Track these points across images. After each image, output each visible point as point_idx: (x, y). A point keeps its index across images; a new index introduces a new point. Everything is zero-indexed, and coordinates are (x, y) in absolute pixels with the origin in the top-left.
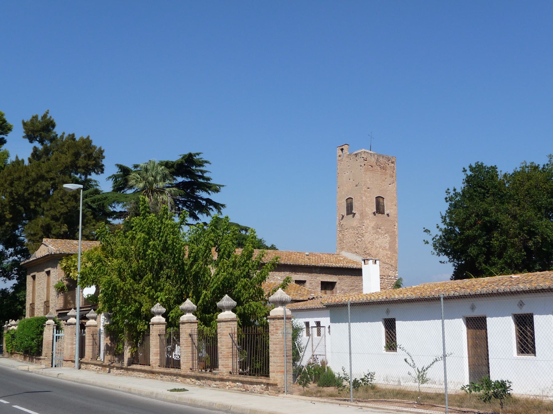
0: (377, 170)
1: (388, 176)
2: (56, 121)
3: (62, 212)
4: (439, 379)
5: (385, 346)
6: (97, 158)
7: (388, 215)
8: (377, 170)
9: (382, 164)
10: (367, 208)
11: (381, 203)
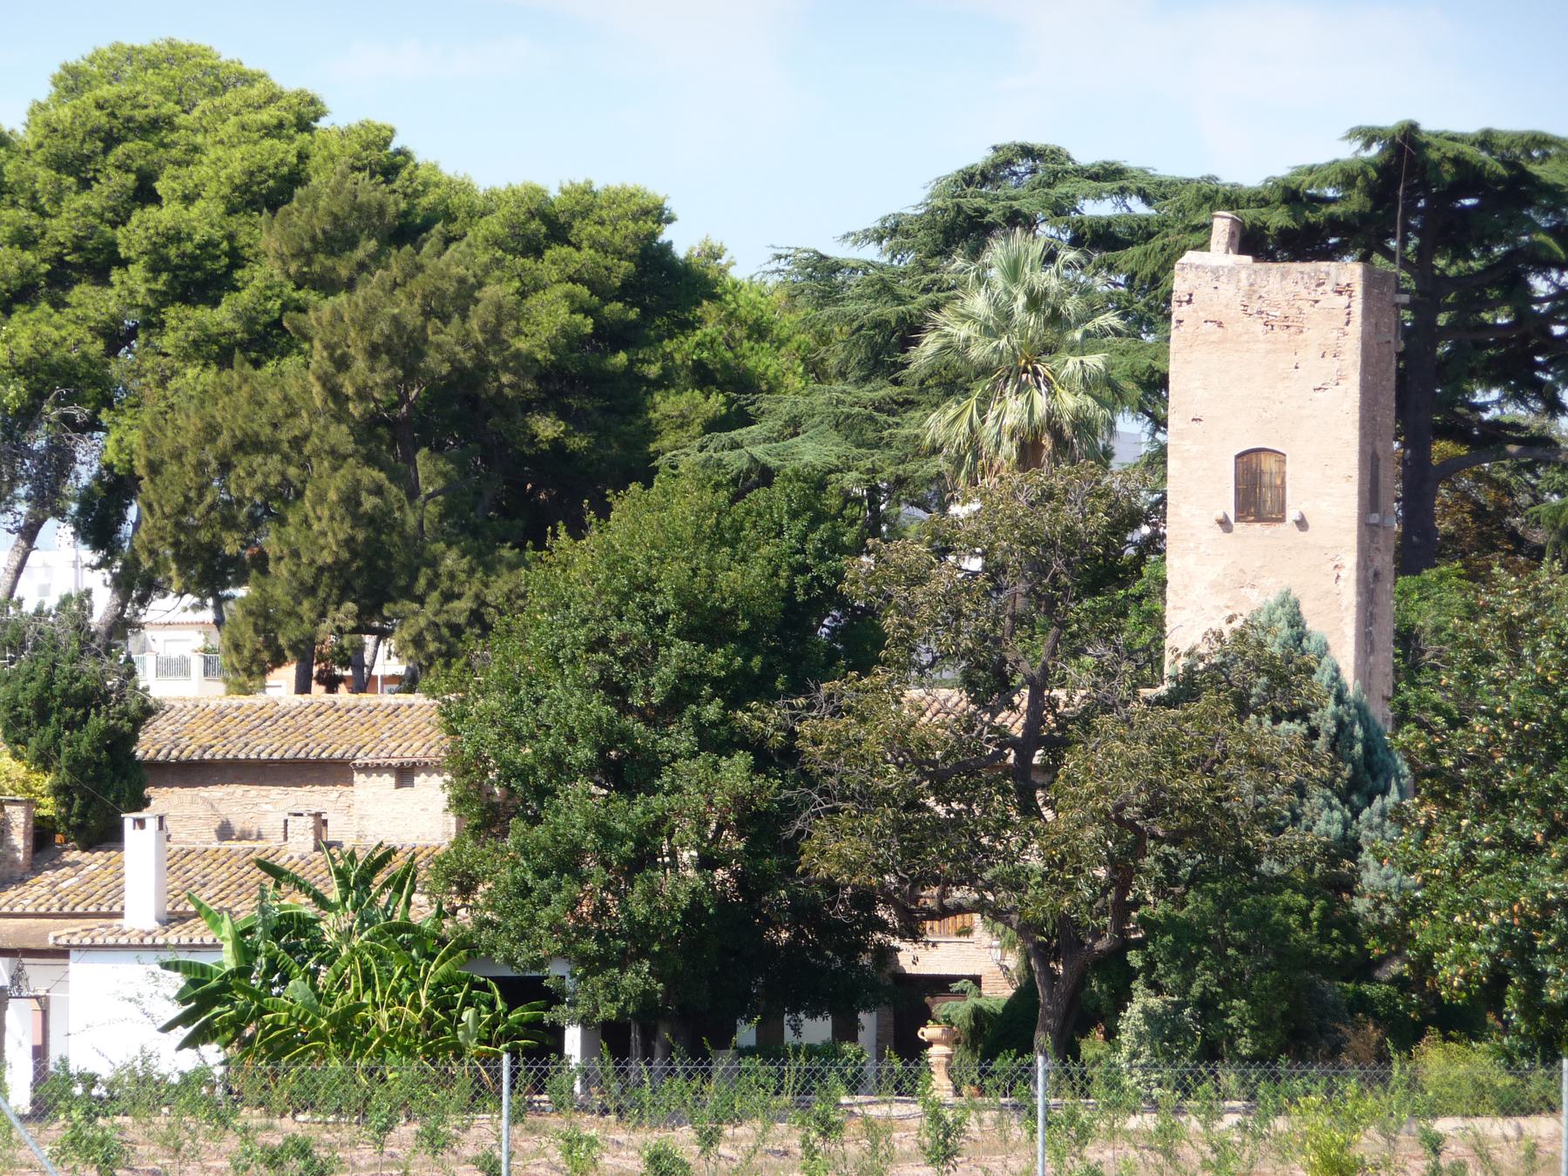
0: (1245, 337)
3: (320, 562)
4: (117, 406)
5: (95, 558)
6: (946, 901)
7: (1302, 524)
8: (1245, 337)
9: (1278, 306)
11: (1266, 479)
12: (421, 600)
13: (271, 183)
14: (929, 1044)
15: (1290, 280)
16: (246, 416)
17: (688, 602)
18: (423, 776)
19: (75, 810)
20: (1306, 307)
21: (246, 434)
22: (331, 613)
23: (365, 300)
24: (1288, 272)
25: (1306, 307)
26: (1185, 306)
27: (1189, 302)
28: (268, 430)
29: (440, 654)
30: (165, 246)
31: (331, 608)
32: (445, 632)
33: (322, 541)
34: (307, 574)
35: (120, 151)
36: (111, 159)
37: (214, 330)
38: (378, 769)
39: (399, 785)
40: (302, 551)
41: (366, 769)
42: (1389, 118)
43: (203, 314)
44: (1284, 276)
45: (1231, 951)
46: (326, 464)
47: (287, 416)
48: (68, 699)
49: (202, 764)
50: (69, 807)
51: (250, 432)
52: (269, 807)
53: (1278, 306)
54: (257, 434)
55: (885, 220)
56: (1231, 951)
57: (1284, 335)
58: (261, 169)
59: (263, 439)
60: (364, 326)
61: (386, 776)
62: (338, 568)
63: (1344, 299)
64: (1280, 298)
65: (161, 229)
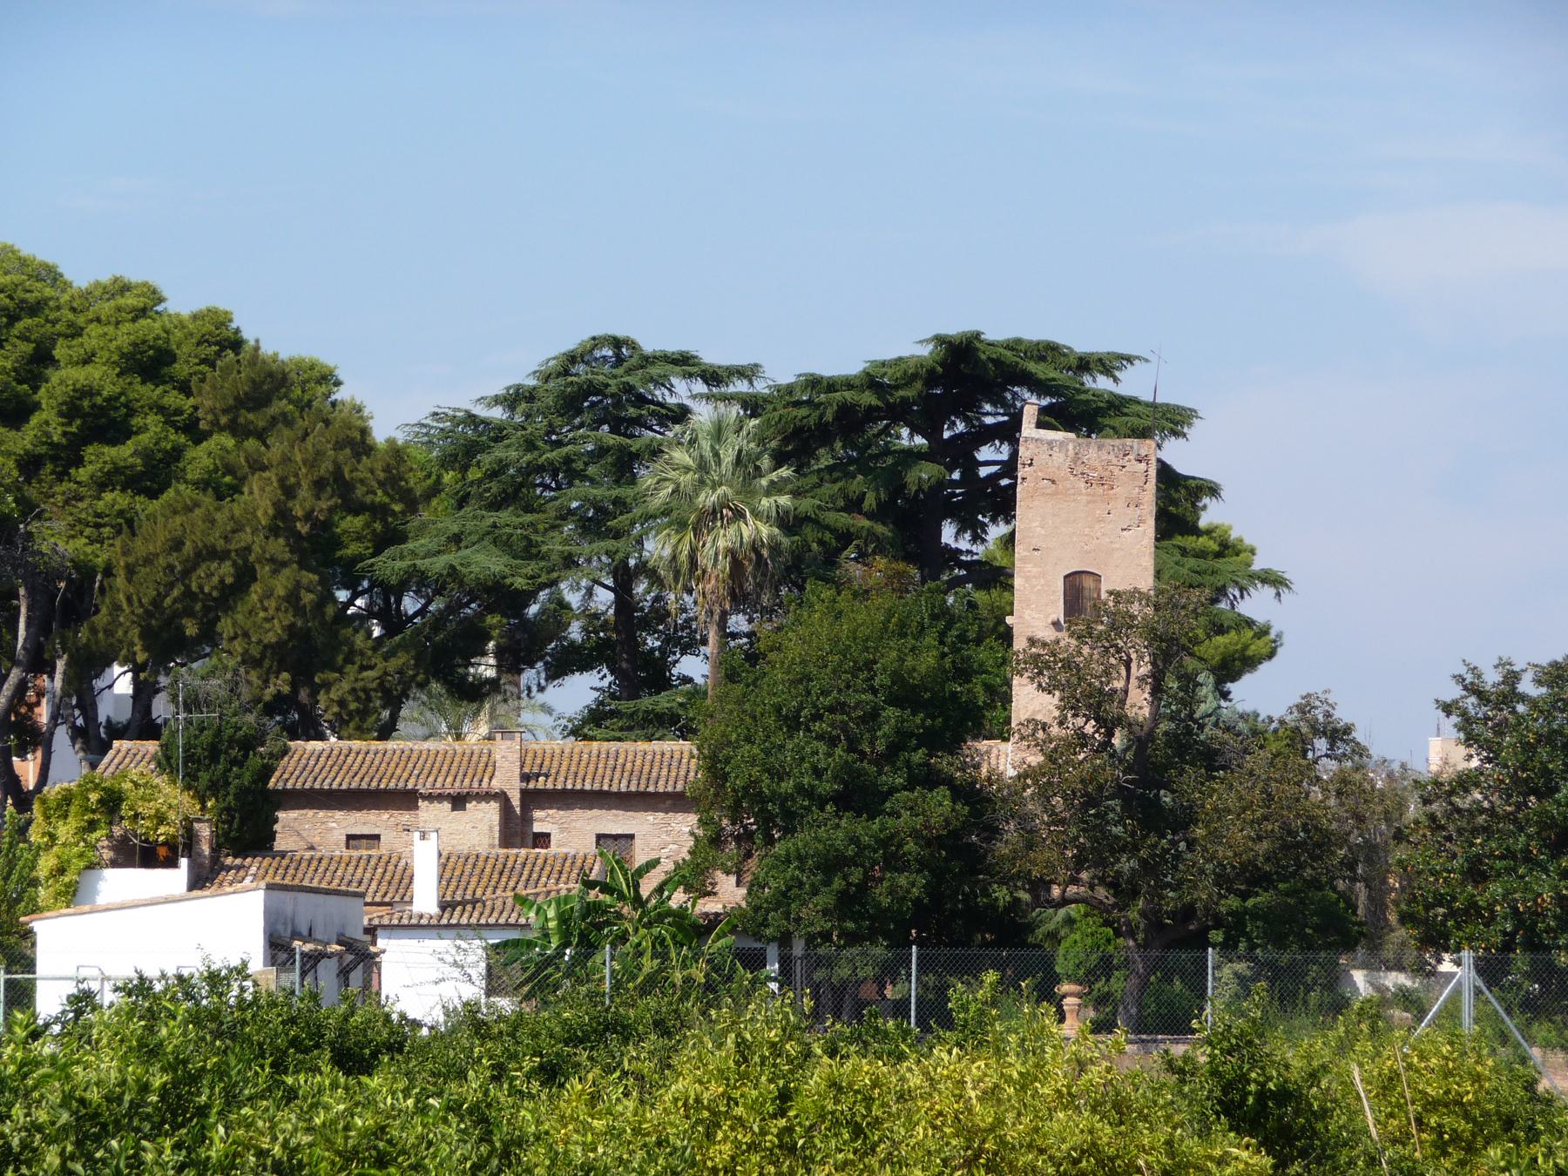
0: (1072, 491)
1: (1121, 504)
2: (222, 305)
3: (266, 641)
8: (1072, 491)
9: (1095, 469)
10: (1028, 612)
11: (1086, 593)
12: (340, 671)
13: (151, 352)
14: (1064, 996)
15: (1104, 452)
16: (203, 531)
17: (897, 677)
18: (474, 803)
19: (235, 826)
20: (1116, 471)
21: (205, 546)
22: (273, 680)
23: (314, 445)
24: (1103, 445)
25: (1116, 471)
26: (1027, 469)
27: (1031, 465)
28: (222, 542)
29: (358, 711)
30: (80, 399)
31: (272, 677)
32: (362, 695)
33: (267, 626)
34: (255, 651)
35: (20, 326)
36: (15, 332)
37: (122, 464)
38: (440, 798)
39: (454, 809)
40: (251, 632)
41: (430, 798)
42: (954, 327)
43: (111, 452)
44: (1100, 448)
45: (1308, 931)
46: (267, 568)
47: (234, 532)
48: (231, 741)
49: (386, 792)
50: (230, 823)
51: (208, 543)
52: (334, 825)
53: (1095, 469)
54: (214, 546)
55: (508, 389)
56: (1308, 931)
57: (1100, 490)
58: (144, 342)
59: (219, 549)
60: (312, 464)
61: (492, 803)
62: (280, 644)
63: (1143, 465)
64: (1097, 464)
65: (78, 386)
